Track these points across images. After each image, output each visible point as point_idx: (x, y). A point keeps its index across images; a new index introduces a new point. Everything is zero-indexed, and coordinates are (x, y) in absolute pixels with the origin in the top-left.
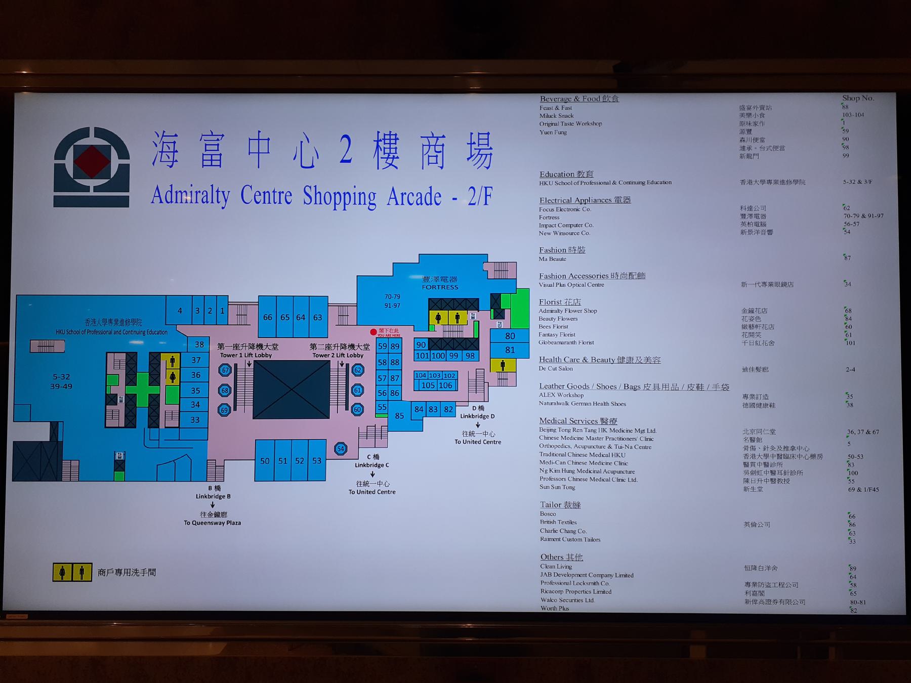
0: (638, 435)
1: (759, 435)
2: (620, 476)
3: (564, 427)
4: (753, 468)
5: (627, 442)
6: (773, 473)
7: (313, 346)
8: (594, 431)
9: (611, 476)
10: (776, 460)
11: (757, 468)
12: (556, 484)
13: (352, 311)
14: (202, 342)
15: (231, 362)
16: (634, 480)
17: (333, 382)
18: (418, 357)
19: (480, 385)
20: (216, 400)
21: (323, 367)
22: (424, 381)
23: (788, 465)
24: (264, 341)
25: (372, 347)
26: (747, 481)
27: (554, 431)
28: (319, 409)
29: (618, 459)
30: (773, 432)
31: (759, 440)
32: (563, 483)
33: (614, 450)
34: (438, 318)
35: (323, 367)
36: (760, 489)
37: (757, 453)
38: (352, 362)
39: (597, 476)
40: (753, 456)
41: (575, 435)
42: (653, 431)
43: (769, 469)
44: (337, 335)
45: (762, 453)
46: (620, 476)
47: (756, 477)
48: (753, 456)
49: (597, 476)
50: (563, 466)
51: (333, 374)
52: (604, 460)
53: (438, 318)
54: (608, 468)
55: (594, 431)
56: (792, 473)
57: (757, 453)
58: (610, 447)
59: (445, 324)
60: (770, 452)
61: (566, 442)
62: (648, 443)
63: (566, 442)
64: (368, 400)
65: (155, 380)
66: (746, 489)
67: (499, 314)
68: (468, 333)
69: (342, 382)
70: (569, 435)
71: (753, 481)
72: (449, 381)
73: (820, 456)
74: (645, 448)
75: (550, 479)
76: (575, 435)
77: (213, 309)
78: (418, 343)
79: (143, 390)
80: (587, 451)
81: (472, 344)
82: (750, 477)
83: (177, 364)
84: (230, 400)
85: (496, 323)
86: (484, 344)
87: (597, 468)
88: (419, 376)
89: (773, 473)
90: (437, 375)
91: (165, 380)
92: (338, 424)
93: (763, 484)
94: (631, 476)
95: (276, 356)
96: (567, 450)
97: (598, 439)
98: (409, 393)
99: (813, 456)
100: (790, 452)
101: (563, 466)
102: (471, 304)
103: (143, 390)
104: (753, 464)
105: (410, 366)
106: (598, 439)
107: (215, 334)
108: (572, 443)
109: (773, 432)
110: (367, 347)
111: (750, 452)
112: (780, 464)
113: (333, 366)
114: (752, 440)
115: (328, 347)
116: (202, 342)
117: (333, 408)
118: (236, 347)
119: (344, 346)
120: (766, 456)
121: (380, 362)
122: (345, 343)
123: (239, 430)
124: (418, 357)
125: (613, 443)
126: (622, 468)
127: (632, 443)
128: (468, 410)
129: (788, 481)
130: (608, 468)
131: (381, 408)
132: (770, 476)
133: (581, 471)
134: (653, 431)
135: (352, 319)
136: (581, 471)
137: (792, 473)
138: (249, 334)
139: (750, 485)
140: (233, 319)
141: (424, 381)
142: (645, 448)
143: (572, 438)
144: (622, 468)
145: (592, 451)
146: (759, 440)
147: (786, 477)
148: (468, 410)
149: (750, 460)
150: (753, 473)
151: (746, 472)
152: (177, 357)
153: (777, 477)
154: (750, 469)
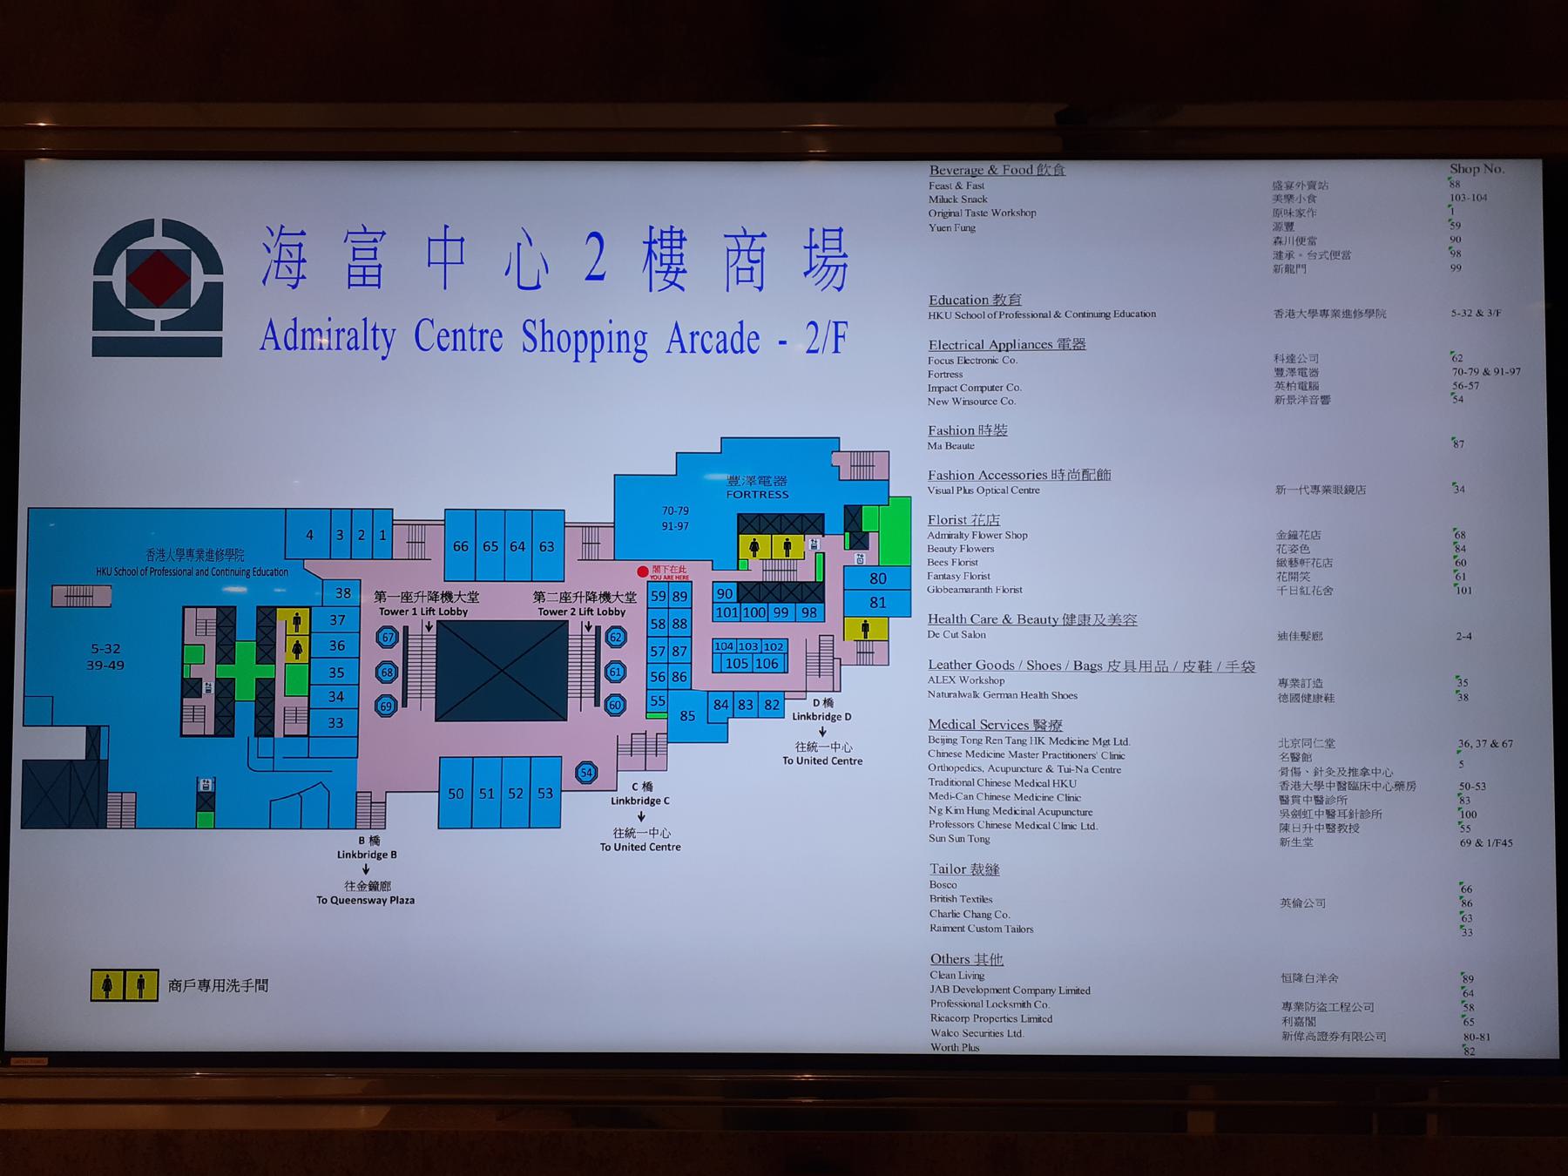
0: (1099, 749)
1: (1306, 750)
2: (1068, 820)
3: (970, 735)
4: (1296, 807)
5: (1079, 762)
6: (1330, 814)
7: (539, 596)
8: (1023, 743)
9: (1052, 819)
10: (1335, 792)
11: (1303, 806)
12: (957, 833)
13: (606, 536)
14: (348, 589)
15: (398, 623)
16: (1091, 827)
17: (573, 658)
18: (719, 615)
19: (826, 663)
20: (371, 688)
21: (556, 631)
22: (729, 655)
23: (1356, 800)
24: (454, 588)
25: (641, 598)
26: (1286, 828)
27: (954, 742)
28: (549, 705)
29: (1064, 790)
30: (1330, 743)
31: (1306, 757)
32: (969, 831)
33: (1057, 775)
34: (754, 547)
35: (556, 631)
36: (1308, 842)
37: (1302, 779)
38: (606, 623)
39: (1028, 820)
40: (1297, 785)
41: (990, 748)
42: (1125, 743)
43: (1323, 808)
44: (581, 576)
45: (1312, 780)
46: (1068, 820)
47: (1302, 821)
48: (1297, 785)
49: (1028, 820)
50: (970, 803)
51: (573, 644)
52: (1039, 791)
53: (754, 547)
54: (1047, 806)
55: (1023, 743)
56: (1363, 814)
57: (1302, 779)
58: (1049, 770)
59: (766, 558)
60: (1325, 779)
61: (975, 762)
62: (1115, 764)
63: (975, 762)
64: (634, 688)
65: (266, 654)
66: (1283, 842)
67: (859, 540)
68: (805, 574)
69: (589, 658)
70: (979, 749)
71: (1296, 829)
72: (773, 656)
73: (1412, 785)
74: (1111, 771)
75: (947, 825)
76: (990, 748)
77: (366, 531)
78: (719, 591)
79: (246, 672)
80: (1011, 777)
81: (812, 593)
82: (1290, 821)
83: (304, 627)
84: (395, 689)
85: (855, 556)
86: (833, 593)
87: (1027, 805)
88: (721, 647)
89: (1330, 814)
90: (752, 645)
91: (283, 654)
92: (582, 730)
93: (1314, 834)
94: (1086, 820)
95: (476, 613)
96: (976, 775)
97: (1030, 755)
98: (704, 677)
99: (1399, 785)
100: (1359, 779)
101: (970, 803)
102: (811, 524)
103: (246, 672)
104: (1296, 799)
105: (706, 629)
106: (1030, 755)
107: (371, 574)
108: (984, 763)
109: (1330, 743)
110: (631, 597)
111: (1290, 779)
112: (1342, 799)
113: (574, 629)
114: (1294, 757)
115: (565, 597)
116: (348, 589)
117: (572, 703)
118: (406, 597)
119: (591, 597)
120: (1319, 785)
121: (654, 624)
122: (594, 591)
123: (411, 741)
124: (719, 615)
125: (1054, 763)
126: (1071, 806)
127: (1087, 763)
128: (805, 707)
129: (1356, 828)
130: (1047, 806)
131: (655, 703)
132: (1324, 820)
133: (1000, 811)
134: (1125, 743)
135: (606, 550)
136: (1000, 811)
137: (1363, 814)
138: (429, 576)
139: (1290, 835)
140: (400, 549)
141: (729, 655)
142: (1111, 771)
143: (985, 755)
144: (1071, 806)
145: (1019, 776)
146: (1306, 757)
147: (1353, 821)
148: (805, 707)
149: (1290, 793)
150: (1295, 814)
151: (1284, 813)
152: (304, 614)
153: (1337, 821)
154: (1291, 807)
